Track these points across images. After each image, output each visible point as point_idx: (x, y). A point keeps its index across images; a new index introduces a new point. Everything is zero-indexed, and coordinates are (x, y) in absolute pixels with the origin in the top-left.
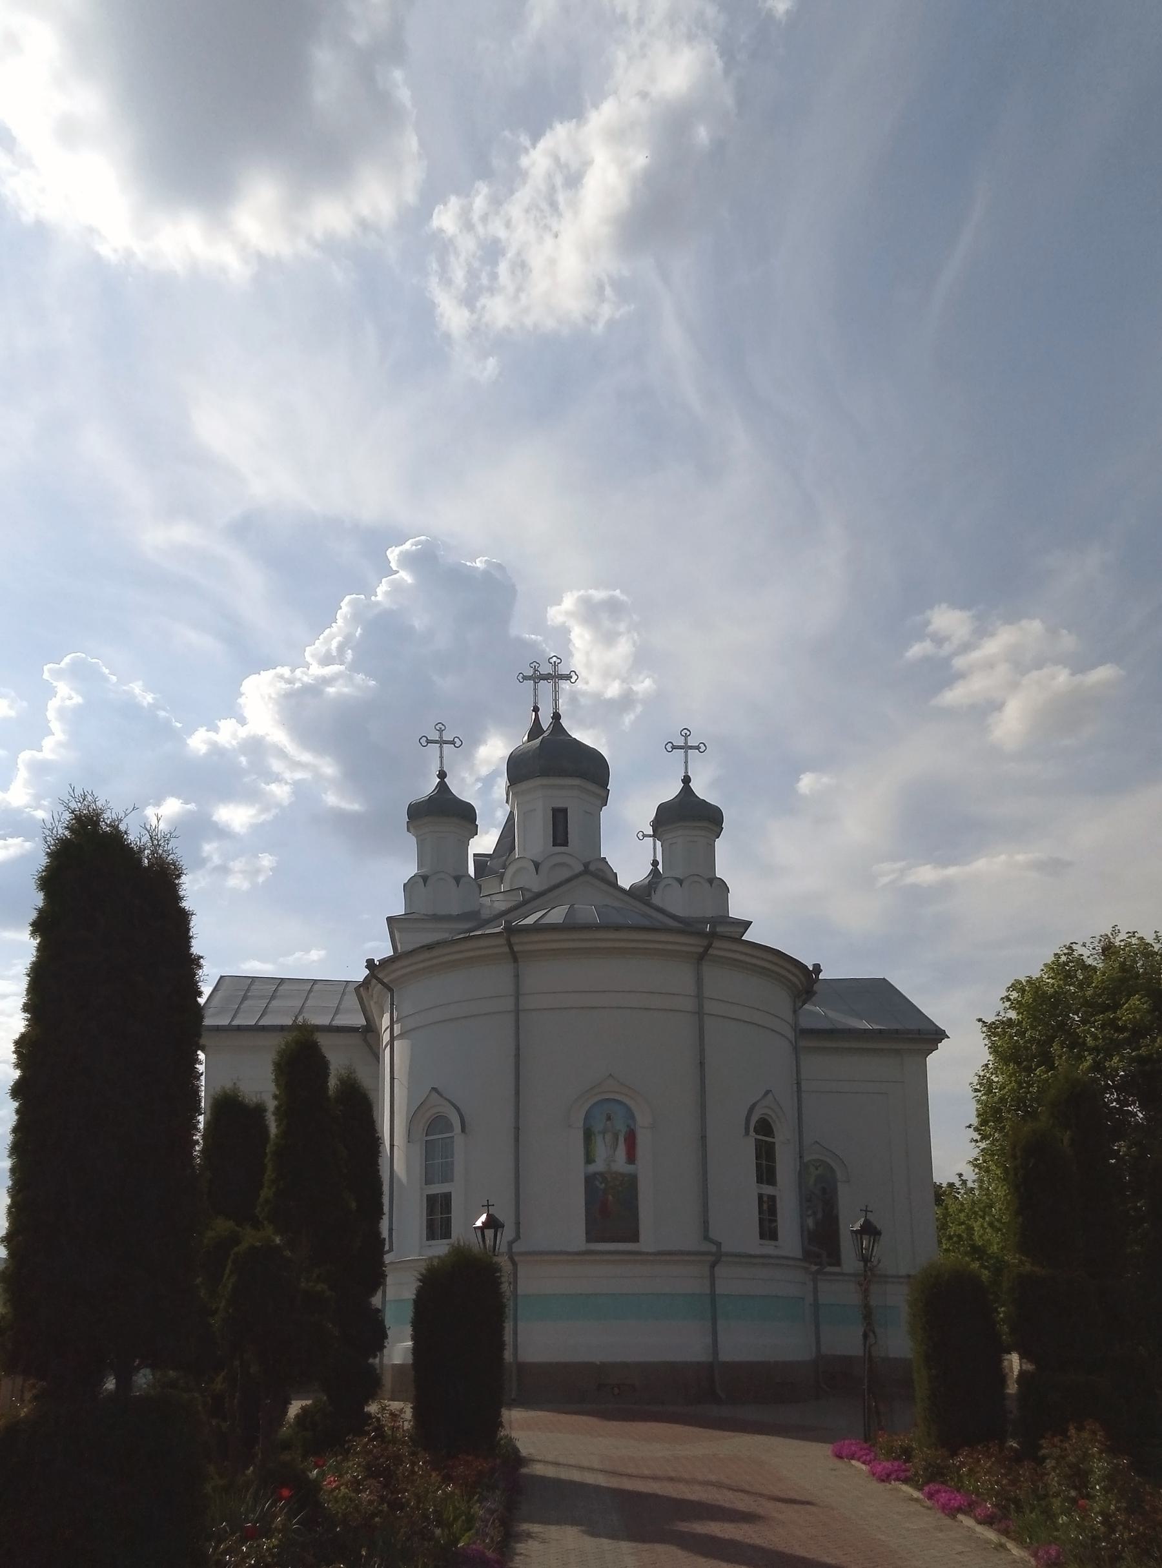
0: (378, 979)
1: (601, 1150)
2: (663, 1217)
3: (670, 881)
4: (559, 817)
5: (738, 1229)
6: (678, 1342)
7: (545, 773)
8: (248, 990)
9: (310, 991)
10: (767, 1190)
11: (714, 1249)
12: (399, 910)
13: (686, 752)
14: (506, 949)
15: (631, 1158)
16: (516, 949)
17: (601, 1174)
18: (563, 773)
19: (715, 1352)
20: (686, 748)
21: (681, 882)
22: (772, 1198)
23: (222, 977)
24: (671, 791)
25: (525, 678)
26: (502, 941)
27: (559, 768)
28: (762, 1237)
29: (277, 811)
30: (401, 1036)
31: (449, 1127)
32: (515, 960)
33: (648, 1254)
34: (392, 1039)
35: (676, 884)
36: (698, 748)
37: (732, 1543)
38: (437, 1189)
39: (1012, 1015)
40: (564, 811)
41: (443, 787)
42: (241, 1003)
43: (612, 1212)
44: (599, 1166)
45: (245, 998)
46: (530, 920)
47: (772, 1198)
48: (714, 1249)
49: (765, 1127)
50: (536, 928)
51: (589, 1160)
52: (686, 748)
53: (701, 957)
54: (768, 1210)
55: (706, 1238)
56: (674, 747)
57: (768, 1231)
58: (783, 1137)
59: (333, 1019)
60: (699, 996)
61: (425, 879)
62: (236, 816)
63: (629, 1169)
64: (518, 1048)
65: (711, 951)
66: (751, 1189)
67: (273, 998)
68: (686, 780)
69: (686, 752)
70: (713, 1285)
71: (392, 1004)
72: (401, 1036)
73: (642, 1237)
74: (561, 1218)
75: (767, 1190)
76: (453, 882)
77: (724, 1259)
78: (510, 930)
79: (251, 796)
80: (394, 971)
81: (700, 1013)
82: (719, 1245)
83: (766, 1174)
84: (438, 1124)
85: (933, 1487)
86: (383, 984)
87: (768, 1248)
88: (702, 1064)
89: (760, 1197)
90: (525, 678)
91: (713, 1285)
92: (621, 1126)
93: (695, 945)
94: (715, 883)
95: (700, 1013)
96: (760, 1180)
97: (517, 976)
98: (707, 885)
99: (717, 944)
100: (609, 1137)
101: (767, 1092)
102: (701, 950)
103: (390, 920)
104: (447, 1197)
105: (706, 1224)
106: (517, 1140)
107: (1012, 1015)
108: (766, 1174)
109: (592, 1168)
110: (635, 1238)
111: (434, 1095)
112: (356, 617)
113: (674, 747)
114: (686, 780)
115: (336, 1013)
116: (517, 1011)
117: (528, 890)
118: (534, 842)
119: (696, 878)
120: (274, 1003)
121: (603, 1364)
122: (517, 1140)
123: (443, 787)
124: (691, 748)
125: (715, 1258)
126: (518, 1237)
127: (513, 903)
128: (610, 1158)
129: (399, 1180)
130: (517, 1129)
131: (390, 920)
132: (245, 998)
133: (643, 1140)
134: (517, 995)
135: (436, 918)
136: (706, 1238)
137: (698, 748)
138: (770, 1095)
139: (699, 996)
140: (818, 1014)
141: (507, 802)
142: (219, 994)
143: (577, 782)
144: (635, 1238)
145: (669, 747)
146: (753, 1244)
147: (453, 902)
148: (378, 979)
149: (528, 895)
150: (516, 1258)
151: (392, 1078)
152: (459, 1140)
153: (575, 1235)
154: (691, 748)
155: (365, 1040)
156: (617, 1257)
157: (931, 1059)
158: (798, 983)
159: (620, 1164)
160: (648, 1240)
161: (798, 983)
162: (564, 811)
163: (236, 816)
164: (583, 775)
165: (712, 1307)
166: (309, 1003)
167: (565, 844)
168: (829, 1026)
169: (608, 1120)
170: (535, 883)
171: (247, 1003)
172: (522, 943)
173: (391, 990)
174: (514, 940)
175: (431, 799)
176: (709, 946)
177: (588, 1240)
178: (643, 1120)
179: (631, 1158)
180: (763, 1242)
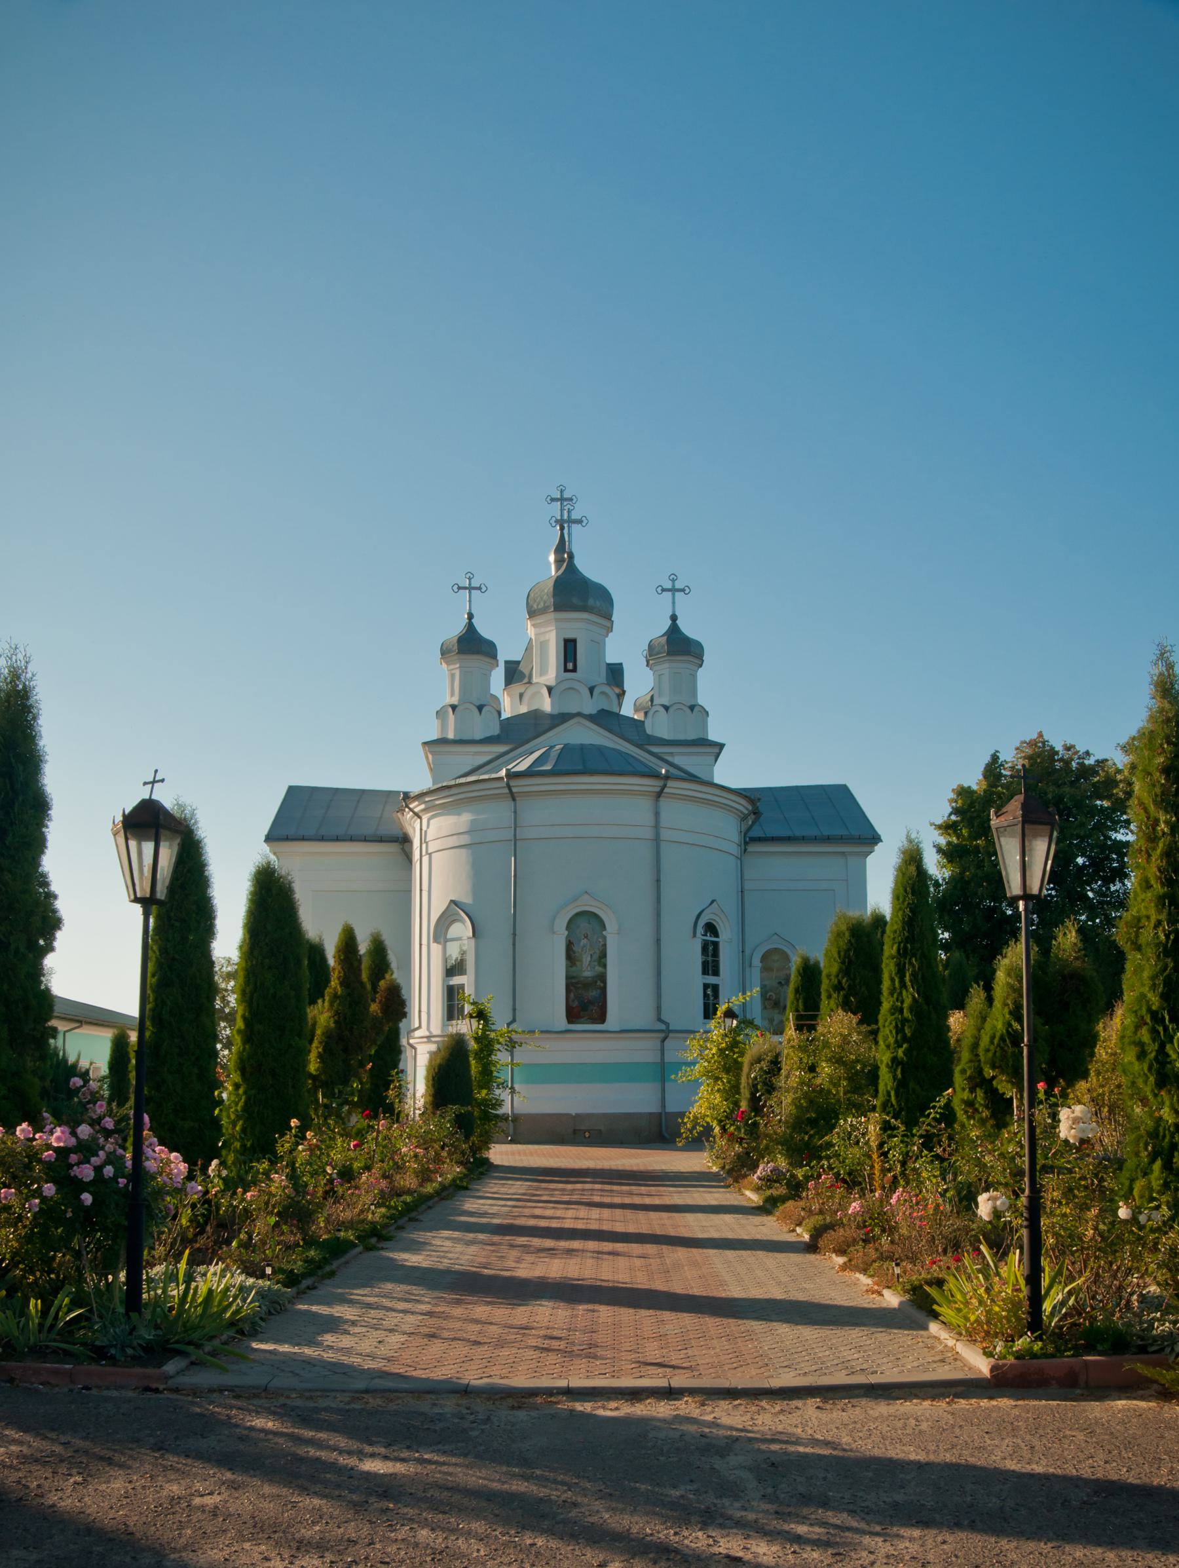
2: (625, 998)
4: (569, 648)
7: (347, 944)
10: (712, 980)
11: (663, 1027)
14: (506, 791)
16: (514, 790)
19: (663, 1105)
21: (666, 708)
25: (553, 500)
32: (514, 799)
35: (662, 710)
37: (483, 1224)
40: (574, 641)
41: (470, 627)
43: (586, 1003)
49: (711, 928)
55: (660, 1020)
60: (657, 826)
65: (666, 790)
66: (698, 980)
68: (674, 618)
75: (712, 980)
76: (476, 711)
81: (657, 840)
82: (667, 1024)
83: (711, 966)
88: (658, 881)
90: (553, 500)
91: (663, 1054)
93: (652, 785)
94: (696, 709)
95: (657, 840)
96: (705, 972)
98: (688, 711)
99: (670, 783)
101: (713, 902)
102: (658, 789)
105: (659, 1008)
108: (711, 966)
113: (663, 590)
114: (674, 618)
121: (578, 1115)
123: (470, 627)
125: (665, 1033)
130: (514, 934)
137: (683, 590)
139: (657, 826)
142: (268, 1355)
145: (659, 590)
155: (403, 850)
157: (870, 860)
162: (574, 641)
167: (574, 670)
174: (512, 783)
176: (665, 786)
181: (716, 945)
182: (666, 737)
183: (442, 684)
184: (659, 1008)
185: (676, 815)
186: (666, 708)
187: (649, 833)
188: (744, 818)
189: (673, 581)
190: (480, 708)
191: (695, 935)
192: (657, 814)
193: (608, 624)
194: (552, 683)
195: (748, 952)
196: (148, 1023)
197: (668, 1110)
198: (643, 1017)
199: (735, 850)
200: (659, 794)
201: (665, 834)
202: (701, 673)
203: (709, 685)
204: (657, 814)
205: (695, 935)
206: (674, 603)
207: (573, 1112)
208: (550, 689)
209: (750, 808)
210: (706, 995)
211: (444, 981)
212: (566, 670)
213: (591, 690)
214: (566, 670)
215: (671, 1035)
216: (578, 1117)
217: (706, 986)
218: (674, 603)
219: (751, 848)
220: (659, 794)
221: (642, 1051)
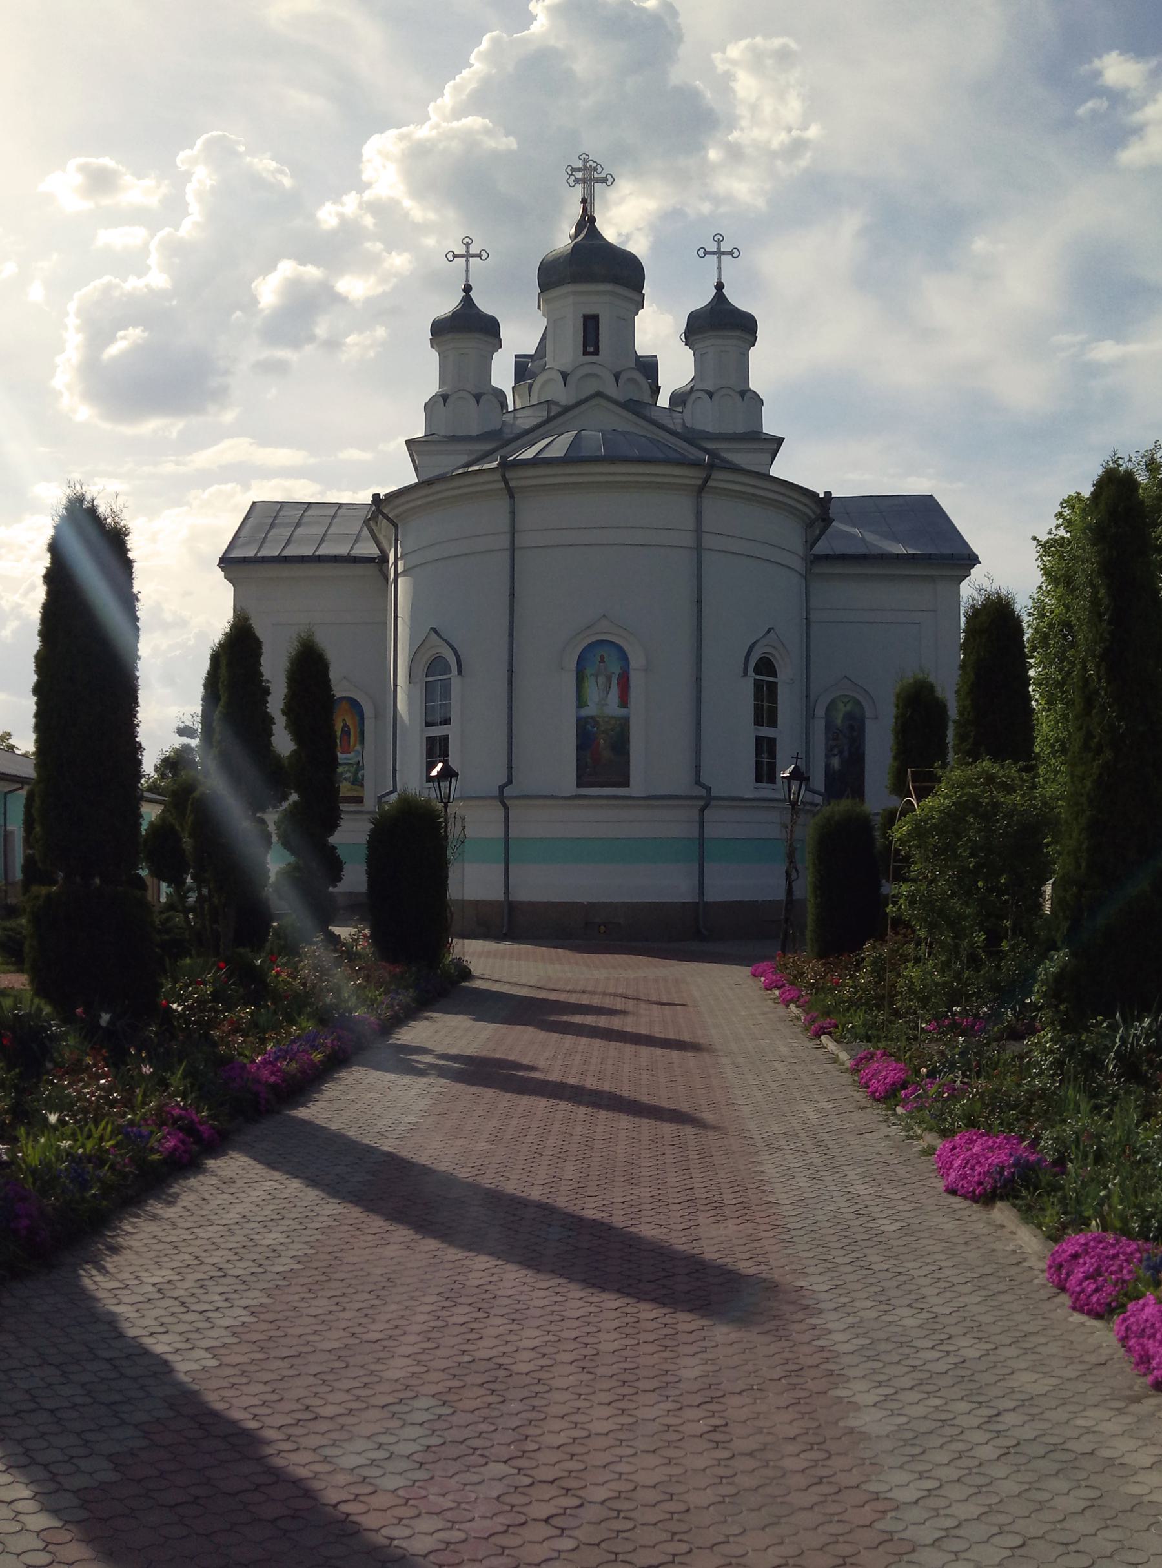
0: (384, 515)
1: (593, 691)
2: (656, 759)
3: (699, 394)
4: (591, 324)
5: (733, 770)
6: (669, 884)
7: (576, 279)
8: (275, 518)
9: (334, 516)
10: (766, 732)
11: (703, 792)
12: (420, 433)
13: (719, 259)
15: (624, 702)
16: (512, 484)
17: (592, 717)
18: (591, 278)
19: (702, 893)
20: (719, 253)
21: (711, 395)
22: (772, 741)
23: (254, 503)
24: (702, 298)
26: (497, 476)
27: (596, 273)
28: (758, 779)
29: (395, 280)
30: (405, 573)
31: (447, 670)
33: (638, 798)
34: (396, 575)
35: (706, 397)
36: (731, 253)
38: (437, 731)
39: (1062, 532)
41: (467, 301)
42: (268, 532)
43: (602, 757)
44: (590, 710)
45: (272, 525)
46: (529, 454)
47: (772, 741)
48: (703, 792)
49: (766, 666)
50: (535, 462)
51: (581, 703)
52: (719, 253)
53: (701, 490)
54: (766, 748)
55: (698, 782)
56: (706, 253)
57: (765, 772)
58: (787, 676)
59: (352, 549)
60: (698, 531)
61: (445, 397)
62: (354, 287)
63: (621, 712)
64: (512, 588)
66: (746, 732)
67: (298, 525)
68: (720, 286)
69: (719, 259)
70: (702, 827)
71: (396, 540)
72: (405, 573)
73: (633, 781)
74: (554, 759)
75: (766, 732)
76: (473, 402)
77: (713, 803)
78: (505, 465)
79: (369, 264)
80: (398, 506)
81: (698, 548)
82: (709, 789)
83: (766, 714)
84: (436, 665)
85: (866, 1047)
86: (389, 519)
87: (766, 791)
88: (699, 601)
89: (758, 738)
91: (702, 827)
92: (615, 669)
93: (693, 477)
94: (748, 395)
95: (698, 548)
96: (758, 722)
97: (513, 513)
99: (716, 475)
100: (602, 680)
101: (769, 631)
102: (700, 482)
103: (408, 442)
104: (445, 739)
105: (698, 769)
106: (510, 683)
107: (1062, 532)
109: (585, 712)
110: (626, 784)
111: (433, 635)
112: (496, 53)
113: (706, 253)
114: (720, 286)
115: (356, 541)
116: (513, 549)
117: (557, 403)
118: (567, 353)
119: (725, 391)
120: (299, 531)
122: (510, 683)
123: (467, 301)
124: (725, 253)
125: (706, 801)
126: (510, 782)
127: (540, 420)
128: (603, 702)
129: (402, 720)
131: (408, 442)
132: (272, 525)
133: (636, 679)
134: (513, 531)
135: (454, 439)
136: (698, 782)
137: (731, 253)
138: (772, 633)
139: (698, 531)
140: (854, 536)
141: (539, 308)
143: (609, 287)
144: (626, 784)
145: (701, 253)
146: (743, 781)
147: (473, 421)
148: (384, 515)
149: (555, 410)
150: (508, 802)
151: (396, 617)
152: (456, 683)
153: (565, 776)
154: (725, 253)
156: (604, 802)
158: (811, 514)
159: (613, 707)
160: (637, 787)
161: (811, 514)
163: (354, 287)
164: (616, 280)
165: (700, 849)
166: (332, 530)
168: (862, 551)
169: (601, 660)
170: (562, 395)
171: (274, 531)
172: (518, 479)
173: (396, 526)
175: (455, 315)
177: (578, 786)
178: (636, 662)
179: (624, 702)
180: (759, 784)
181: (773, 687)
182: (710, 429)
183: (424, 374)
184: (698, 769)
185: (720, 514)
186: (711, 395)
187: (688, 540)
188: (810, 525)
189: (719, 242)
190: (478, 397)
191: (745, 674)
192: (698, 514)
193: (638, 298)
194: (567, 368)
195: (812, 698)
196: (36, 799)
197: (709, 898)
198: (678, 780)
199: (798, 564)
200: (701, 490)
201: (708, 541)
202: (753, 353)
203: (765, 367)
204: (698, 514)
205: (745, 674)
206: (719, 268)
207: (585, 899)
208: (565, 376)
209: (818, 511)
210: (758, 753)
211: (422, 731)
212: (585, 353)
213: (617, 377)
214: (585, 353)
215: (713, 803)
216: (592, 906)
217: (759, 739)
218: (719, 268)
219: (817, 570)
220: (701, 490)
221: (675, 824)
